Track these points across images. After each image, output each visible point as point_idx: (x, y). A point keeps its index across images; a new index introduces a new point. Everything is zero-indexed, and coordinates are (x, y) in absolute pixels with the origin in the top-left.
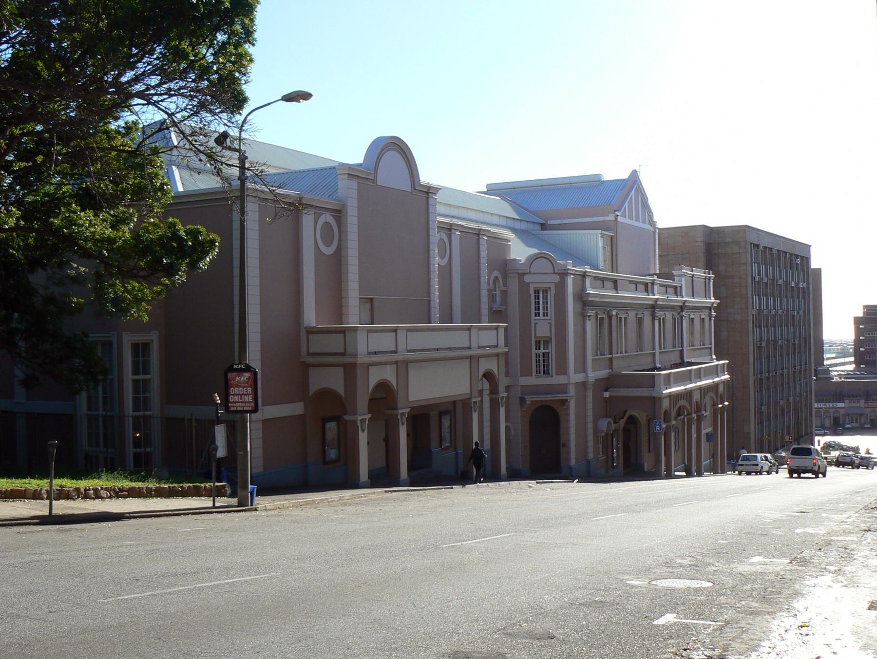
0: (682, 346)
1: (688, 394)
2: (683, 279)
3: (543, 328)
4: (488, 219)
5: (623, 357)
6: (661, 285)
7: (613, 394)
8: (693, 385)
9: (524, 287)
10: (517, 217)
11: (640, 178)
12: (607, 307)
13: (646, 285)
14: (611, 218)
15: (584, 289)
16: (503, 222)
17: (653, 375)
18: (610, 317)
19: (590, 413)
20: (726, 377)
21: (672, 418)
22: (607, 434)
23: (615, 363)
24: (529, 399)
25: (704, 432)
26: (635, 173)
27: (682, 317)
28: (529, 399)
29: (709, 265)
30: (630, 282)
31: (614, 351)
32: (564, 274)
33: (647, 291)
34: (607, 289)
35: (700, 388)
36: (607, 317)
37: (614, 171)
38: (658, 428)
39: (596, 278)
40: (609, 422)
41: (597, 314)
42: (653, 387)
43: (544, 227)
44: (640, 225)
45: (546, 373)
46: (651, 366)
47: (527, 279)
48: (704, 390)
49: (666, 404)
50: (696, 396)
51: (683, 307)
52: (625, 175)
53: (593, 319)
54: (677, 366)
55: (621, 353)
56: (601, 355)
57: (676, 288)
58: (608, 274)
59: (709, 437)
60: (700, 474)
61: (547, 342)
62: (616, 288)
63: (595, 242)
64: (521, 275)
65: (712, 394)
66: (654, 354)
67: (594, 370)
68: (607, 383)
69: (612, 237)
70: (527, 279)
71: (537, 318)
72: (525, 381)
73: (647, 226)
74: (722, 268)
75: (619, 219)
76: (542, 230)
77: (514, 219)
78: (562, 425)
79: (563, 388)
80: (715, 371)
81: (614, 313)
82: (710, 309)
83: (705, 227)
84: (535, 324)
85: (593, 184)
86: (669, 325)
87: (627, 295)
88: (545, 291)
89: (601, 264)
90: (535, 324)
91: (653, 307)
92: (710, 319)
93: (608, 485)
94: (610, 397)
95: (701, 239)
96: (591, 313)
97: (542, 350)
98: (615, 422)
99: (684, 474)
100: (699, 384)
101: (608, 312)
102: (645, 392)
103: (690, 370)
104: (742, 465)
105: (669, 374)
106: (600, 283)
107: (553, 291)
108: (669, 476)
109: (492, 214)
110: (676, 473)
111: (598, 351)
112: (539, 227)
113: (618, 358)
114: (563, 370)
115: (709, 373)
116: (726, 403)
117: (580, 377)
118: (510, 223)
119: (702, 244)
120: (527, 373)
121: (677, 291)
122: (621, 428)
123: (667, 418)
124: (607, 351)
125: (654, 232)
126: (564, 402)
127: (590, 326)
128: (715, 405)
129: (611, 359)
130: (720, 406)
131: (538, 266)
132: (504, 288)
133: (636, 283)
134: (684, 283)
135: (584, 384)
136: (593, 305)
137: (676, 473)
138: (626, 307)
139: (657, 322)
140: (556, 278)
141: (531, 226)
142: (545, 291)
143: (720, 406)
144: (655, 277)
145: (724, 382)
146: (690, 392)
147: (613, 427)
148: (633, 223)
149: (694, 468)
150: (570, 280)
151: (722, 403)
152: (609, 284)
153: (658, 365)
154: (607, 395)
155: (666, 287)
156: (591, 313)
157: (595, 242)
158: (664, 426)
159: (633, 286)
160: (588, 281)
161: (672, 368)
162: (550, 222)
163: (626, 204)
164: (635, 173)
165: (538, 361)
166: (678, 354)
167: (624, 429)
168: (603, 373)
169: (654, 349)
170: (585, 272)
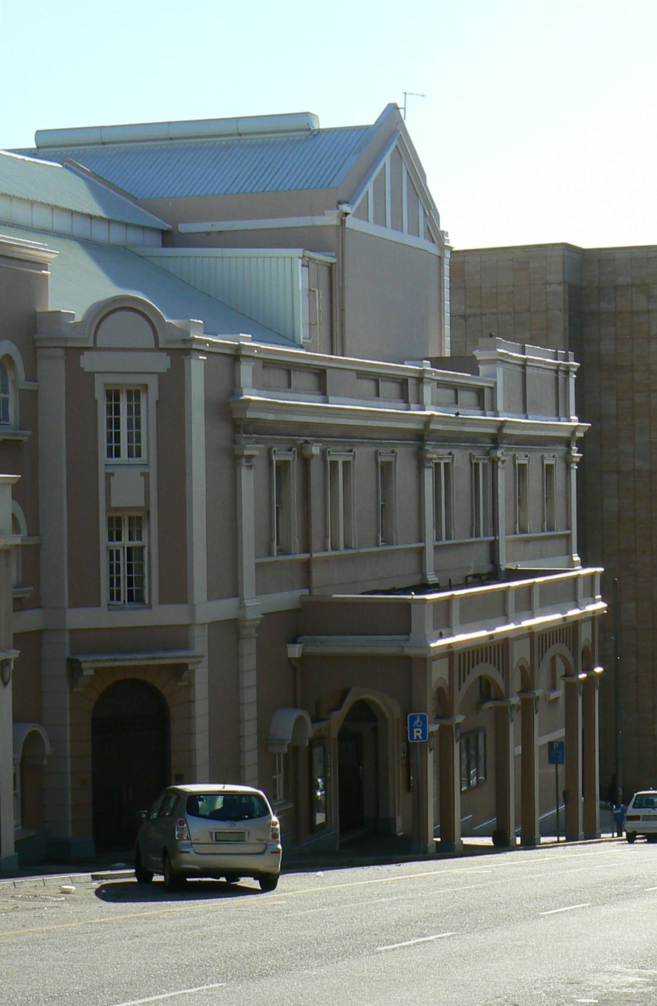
0: (495, 532)
1: (498, 649)
2: (500, 371)
3: (127, 485)
4: (22, 214)
5: (339, 559)
6: (441, 385)
7: (311, 649)
8: (512, 626)
9: (79, 382)
10: (97, 211)
11: (407, 123)
12: (297, 434)
13: (403, 383)
14: (330, 219)
15: (234, 388)
16: (61, 223)
17: (408, 605)
18: (306, 462)
19: (250, 696)
20: (601, 605)
21: (456, 709)
22: (295, 749)
23: (318, 574)
24: (89, 665)
25: (540, 741)
26: (392, 115)
27: (494, 462)
28: (89, 665)
29: (577, 342)
30: (362, 375)
31: (316, 542)
32: (182, 351)
33: (404, 397)
34: (297, 391)
35: (530, 634)
36: (298, 461)
37: (344, 107)
38: (417, 733)
39: (268, 363)
40: (300, 719)
41: (269, 452)
42: (408, 632)
43: (168, 238)
44: (404, 238)
45: (136, 597)
46: (415, 580)
47: (88, 362)
48: (540, 639)
49: (439, 673)
50: (520, 654)
51: (497, 438)
52: (368, 116)
53: (260, 464)
54: (479, 579)
55: (335, 548)
56: (281, 552)
57: (479, 392)
58: (321, 356)
59: (555, 752)
60: (530, 843)
61: (137, 523)
62: (322, 391)
63: (287, 277)
64: (73, 353)
65: (560, 649)
66: (421, 552)
67: (261, 590)
68: (298, 623)
69: (331, 267)
70: (88, 362)
71: (114, 460)
72: (82, 618)
73: (422, 243)
74: (607, 347)
75: (350, 222)
76: (165, 245)
77: (91, 217)
78: (175, 727)
79: (177, 638)
80: (571, 592)
81: (316, 450)
82: (567, 442)
83: (567, 248)
84: (108, 476)
85: (293, 137)
86: (461, 481)
87: (349, 405)
88: (134, 395)
89: (302, 333)
90: (108, 476)
91: (421, 437)
92: (568, 468)
93: (192, 901)
94: (305, 658)
95: (559, 277)
96: (252, 449)
97: (125, 542)
98: (316, 719)
99: (488, 841)
100: (526, 623)
101: (301, 449)
102: (385, 645)
103: (505, 591)
104: (637, 818)
105: (448, 601)
106: (279, 376)
107: (154, 392)
108: (448, 849)
109: (32, 203)
110: (467, 841)
111: (273, 540)
112: (157, 239)
113: (326, 560)
114: (177, 590)
115: (560, 594)
116: (598, 670)
117: (224, 609)
118: (82, 228)
119: (561, 288)
120: (84, 596)
121: (482, 398)
122: (335, 734)
123: (444, 711)
124: (296, 543)
125: (441, 258)
126: (179, 671)
127: (250, 483)
128: (570, 673)
129: (307, 566)
130: (582, 676)
131: (110, 334)
132: (31, 386)
133: (376, 378)
134: (500, 379)
135: (233, 627)
136: (259, 429)
137: (467, 841)
138: (349, 436)
139: (428, 474)
140: (163, 363)
141: (134, 236)
142: (134, 395)
143: (582, 676)
144: (427, 366)
145: (593, 618)
146: (503, 645)
147: (310, 731)
148: (387, 233)
149: (513, 828)
150: (197, 367)
151: (588, 669)
152: (306, 380)
153: (432, 578)
154: (295, 651)
155: (456, 388)
156: (252, 449)
157: (287, 277)
158: (433, 728)
159: (369, 386)
160: (246, 371)
161: (467, 585)
162: (183, 228)
163: (369, 187)
164: (392, 115)
165: (114, 569)
166: (484, 551)
167: (343, 736)
168: (285, 599)
169: (421, 539)
170: (239, 348)
